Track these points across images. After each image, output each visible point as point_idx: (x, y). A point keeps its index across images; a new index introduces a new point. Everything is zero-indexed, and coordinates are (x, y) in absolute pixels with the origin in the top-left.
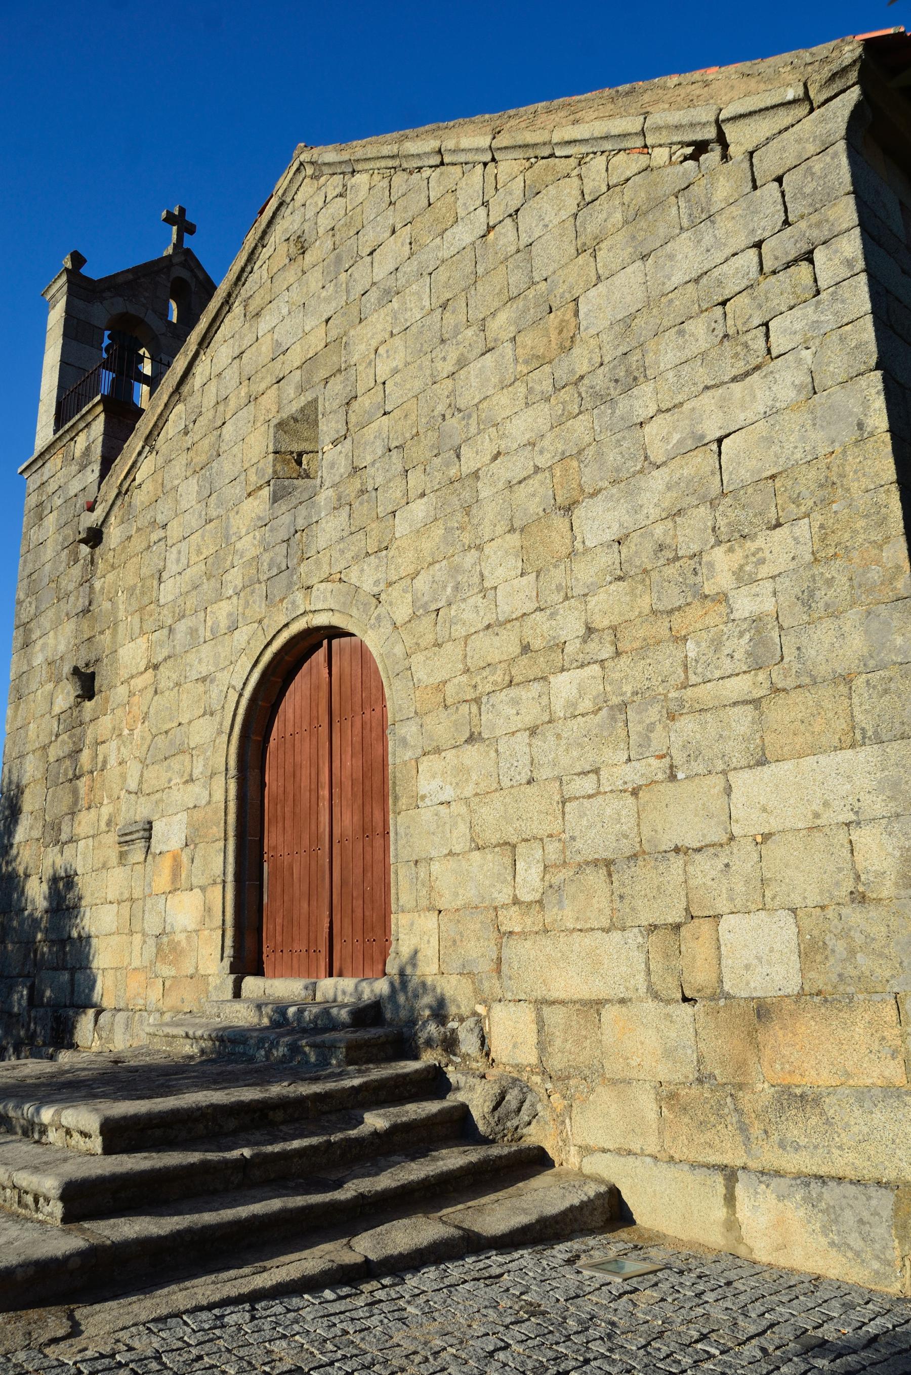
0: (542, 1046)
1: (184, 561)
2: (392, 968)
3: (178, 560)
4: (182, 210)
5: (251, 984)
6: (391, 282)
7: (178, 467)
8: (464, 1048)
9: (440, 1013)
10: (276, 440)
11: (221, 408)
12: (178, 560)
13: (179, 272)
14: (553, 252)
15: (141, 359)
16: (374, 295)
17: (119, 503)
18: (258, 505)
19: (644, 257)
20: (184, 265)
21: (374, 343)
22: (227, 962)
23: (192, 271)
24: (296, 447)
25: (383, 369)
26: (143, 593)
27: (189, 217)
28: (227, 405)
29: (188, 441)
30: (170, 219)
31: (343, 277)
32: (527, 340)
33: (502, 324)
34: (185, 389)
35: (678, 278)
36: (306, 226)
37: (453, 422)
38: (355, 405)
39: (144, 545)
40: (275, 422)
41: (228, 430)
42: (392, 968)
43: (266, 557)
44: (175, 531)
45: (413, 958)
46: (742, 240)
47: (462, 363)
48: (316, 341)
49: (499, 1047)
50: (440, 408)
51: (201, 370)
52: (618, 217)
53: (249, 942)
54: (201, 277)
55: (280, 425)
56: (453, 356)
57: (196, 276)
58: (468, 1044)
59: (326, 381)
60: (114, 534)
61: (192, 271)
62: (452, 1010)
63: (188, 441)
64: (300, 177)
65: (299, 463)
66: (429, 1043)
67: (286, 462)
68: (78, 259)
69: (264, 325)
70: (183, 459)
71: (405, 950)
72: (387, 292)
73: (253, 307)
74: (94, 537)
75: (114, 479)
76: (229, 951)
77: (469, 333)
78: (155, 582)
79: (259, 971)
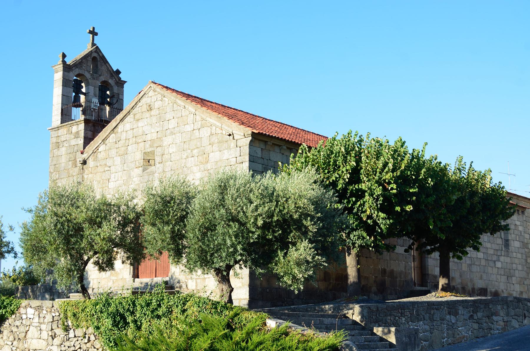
0: (196, 286)
1: (116, 179)
2: (170, 275)
3: (115, 178)
4: (94, 28)
5: (136, 279)
6: (173, 130)
7: (113, 152)
8: (72, 314)
9: (179, 282)
10: (144, 156)
11: (127, 141)
12: (115, 178)
13: (95, 55)
14: (205, 142)
15: (82, 87)
16: (169, 131)
17: (93, 154)
18: (139, 171)
19: (220, 151)
20: (96, 52)
21: (169, 144)
22: (131, 275)
23: (98, 53)
24: (148, 158)
25: (171, 151)
26: (103, 183)
27: (96, 31)
28: (129, 141)
29: (117, 146)
30: (90, 32)
31: (161, 123)
32: (200, 158)
33: (195, 152)
34: (115, 130)
35: (225, 158)
36: (152, 103)
37: (185, 169)
38: (164, 156)
39: (103, 170)
40: (143, 152)
41: (129, 148)
42: (170, 275)
43: (141, 185)
44: (113, 169)
45: (174, 273)
46: (234, 156)
47: (187, 157)
48: (154, 136)
49: (189, 287)
50: (183, 165)
51: (120, 128)
52: (216, 141)
53: (136, 271)
54: (101, 55)
55: (145, 153)
56: (186, 155)
57: (99, 55)
58: (184, 286)
59: (157, 147)
60: (91, 163)
61: (98, 53)
62: (181, 281)
63: (117, 146)
64: (150, 89)
65: (149, 162)
66: (177, 287)
67: (146, 162)
68: (64, 56)
69: (140, 124)
70: (115, 150)
71: (173, 272)
72: (172, 132)
73: (137, 117)
74: (84, 162)
75: (91, 147)
76: (132, 273)
77: (189, 151)
78: (107, 182)
79: (138, 277)
